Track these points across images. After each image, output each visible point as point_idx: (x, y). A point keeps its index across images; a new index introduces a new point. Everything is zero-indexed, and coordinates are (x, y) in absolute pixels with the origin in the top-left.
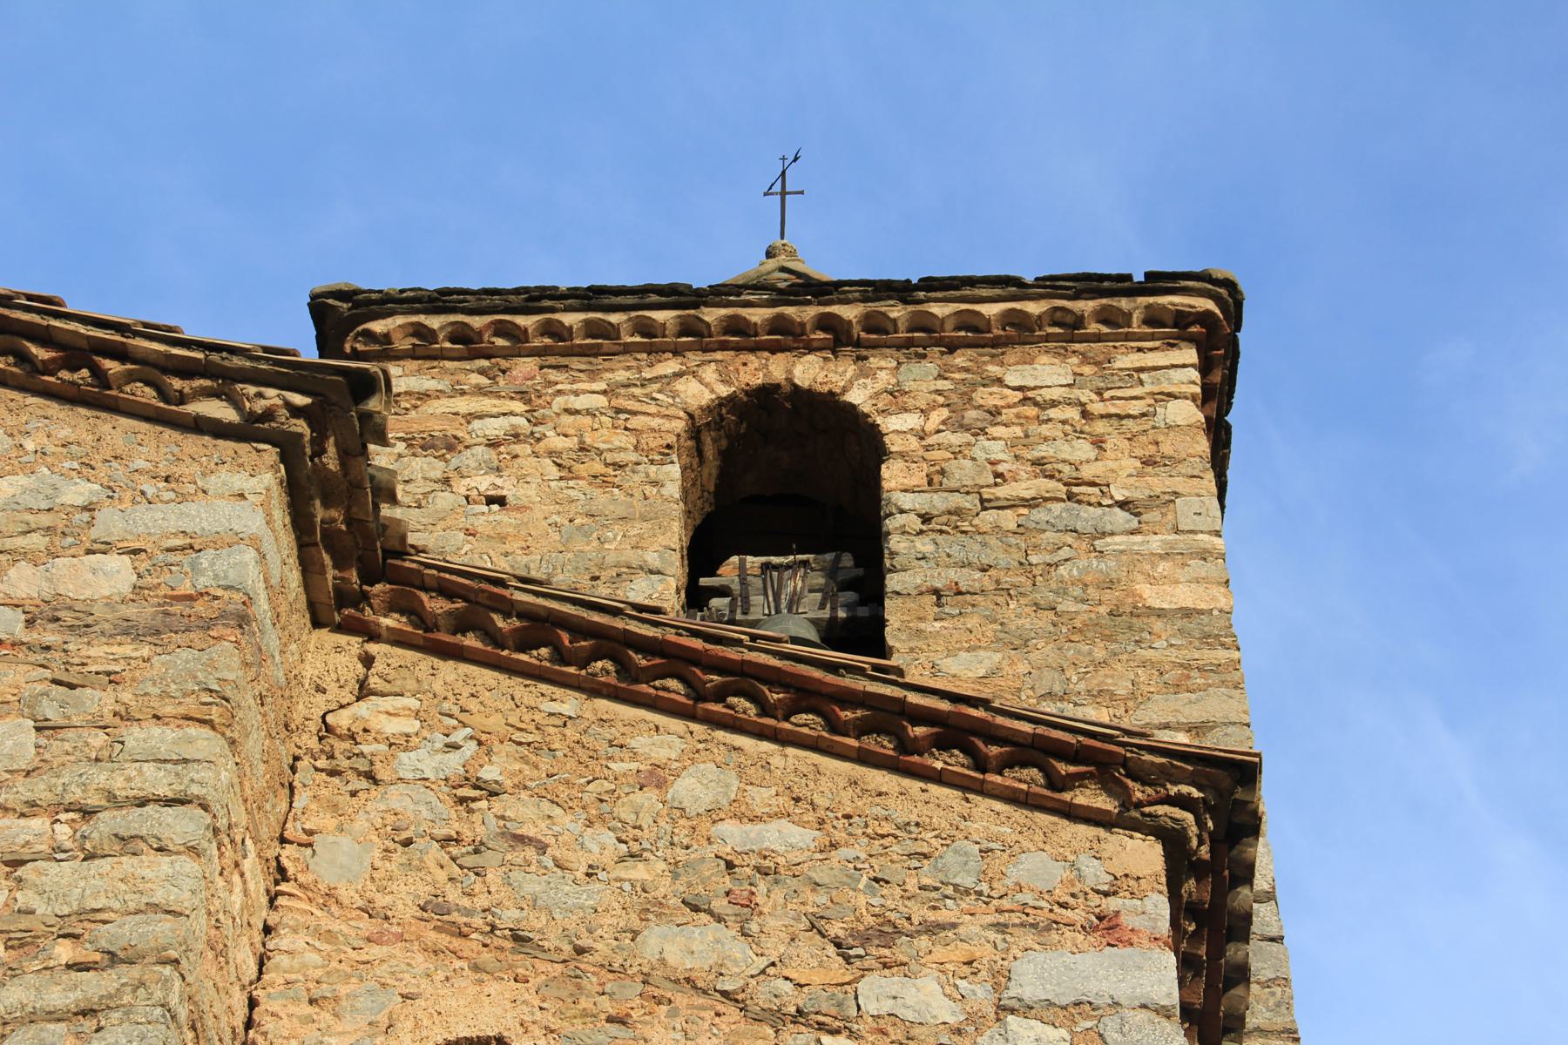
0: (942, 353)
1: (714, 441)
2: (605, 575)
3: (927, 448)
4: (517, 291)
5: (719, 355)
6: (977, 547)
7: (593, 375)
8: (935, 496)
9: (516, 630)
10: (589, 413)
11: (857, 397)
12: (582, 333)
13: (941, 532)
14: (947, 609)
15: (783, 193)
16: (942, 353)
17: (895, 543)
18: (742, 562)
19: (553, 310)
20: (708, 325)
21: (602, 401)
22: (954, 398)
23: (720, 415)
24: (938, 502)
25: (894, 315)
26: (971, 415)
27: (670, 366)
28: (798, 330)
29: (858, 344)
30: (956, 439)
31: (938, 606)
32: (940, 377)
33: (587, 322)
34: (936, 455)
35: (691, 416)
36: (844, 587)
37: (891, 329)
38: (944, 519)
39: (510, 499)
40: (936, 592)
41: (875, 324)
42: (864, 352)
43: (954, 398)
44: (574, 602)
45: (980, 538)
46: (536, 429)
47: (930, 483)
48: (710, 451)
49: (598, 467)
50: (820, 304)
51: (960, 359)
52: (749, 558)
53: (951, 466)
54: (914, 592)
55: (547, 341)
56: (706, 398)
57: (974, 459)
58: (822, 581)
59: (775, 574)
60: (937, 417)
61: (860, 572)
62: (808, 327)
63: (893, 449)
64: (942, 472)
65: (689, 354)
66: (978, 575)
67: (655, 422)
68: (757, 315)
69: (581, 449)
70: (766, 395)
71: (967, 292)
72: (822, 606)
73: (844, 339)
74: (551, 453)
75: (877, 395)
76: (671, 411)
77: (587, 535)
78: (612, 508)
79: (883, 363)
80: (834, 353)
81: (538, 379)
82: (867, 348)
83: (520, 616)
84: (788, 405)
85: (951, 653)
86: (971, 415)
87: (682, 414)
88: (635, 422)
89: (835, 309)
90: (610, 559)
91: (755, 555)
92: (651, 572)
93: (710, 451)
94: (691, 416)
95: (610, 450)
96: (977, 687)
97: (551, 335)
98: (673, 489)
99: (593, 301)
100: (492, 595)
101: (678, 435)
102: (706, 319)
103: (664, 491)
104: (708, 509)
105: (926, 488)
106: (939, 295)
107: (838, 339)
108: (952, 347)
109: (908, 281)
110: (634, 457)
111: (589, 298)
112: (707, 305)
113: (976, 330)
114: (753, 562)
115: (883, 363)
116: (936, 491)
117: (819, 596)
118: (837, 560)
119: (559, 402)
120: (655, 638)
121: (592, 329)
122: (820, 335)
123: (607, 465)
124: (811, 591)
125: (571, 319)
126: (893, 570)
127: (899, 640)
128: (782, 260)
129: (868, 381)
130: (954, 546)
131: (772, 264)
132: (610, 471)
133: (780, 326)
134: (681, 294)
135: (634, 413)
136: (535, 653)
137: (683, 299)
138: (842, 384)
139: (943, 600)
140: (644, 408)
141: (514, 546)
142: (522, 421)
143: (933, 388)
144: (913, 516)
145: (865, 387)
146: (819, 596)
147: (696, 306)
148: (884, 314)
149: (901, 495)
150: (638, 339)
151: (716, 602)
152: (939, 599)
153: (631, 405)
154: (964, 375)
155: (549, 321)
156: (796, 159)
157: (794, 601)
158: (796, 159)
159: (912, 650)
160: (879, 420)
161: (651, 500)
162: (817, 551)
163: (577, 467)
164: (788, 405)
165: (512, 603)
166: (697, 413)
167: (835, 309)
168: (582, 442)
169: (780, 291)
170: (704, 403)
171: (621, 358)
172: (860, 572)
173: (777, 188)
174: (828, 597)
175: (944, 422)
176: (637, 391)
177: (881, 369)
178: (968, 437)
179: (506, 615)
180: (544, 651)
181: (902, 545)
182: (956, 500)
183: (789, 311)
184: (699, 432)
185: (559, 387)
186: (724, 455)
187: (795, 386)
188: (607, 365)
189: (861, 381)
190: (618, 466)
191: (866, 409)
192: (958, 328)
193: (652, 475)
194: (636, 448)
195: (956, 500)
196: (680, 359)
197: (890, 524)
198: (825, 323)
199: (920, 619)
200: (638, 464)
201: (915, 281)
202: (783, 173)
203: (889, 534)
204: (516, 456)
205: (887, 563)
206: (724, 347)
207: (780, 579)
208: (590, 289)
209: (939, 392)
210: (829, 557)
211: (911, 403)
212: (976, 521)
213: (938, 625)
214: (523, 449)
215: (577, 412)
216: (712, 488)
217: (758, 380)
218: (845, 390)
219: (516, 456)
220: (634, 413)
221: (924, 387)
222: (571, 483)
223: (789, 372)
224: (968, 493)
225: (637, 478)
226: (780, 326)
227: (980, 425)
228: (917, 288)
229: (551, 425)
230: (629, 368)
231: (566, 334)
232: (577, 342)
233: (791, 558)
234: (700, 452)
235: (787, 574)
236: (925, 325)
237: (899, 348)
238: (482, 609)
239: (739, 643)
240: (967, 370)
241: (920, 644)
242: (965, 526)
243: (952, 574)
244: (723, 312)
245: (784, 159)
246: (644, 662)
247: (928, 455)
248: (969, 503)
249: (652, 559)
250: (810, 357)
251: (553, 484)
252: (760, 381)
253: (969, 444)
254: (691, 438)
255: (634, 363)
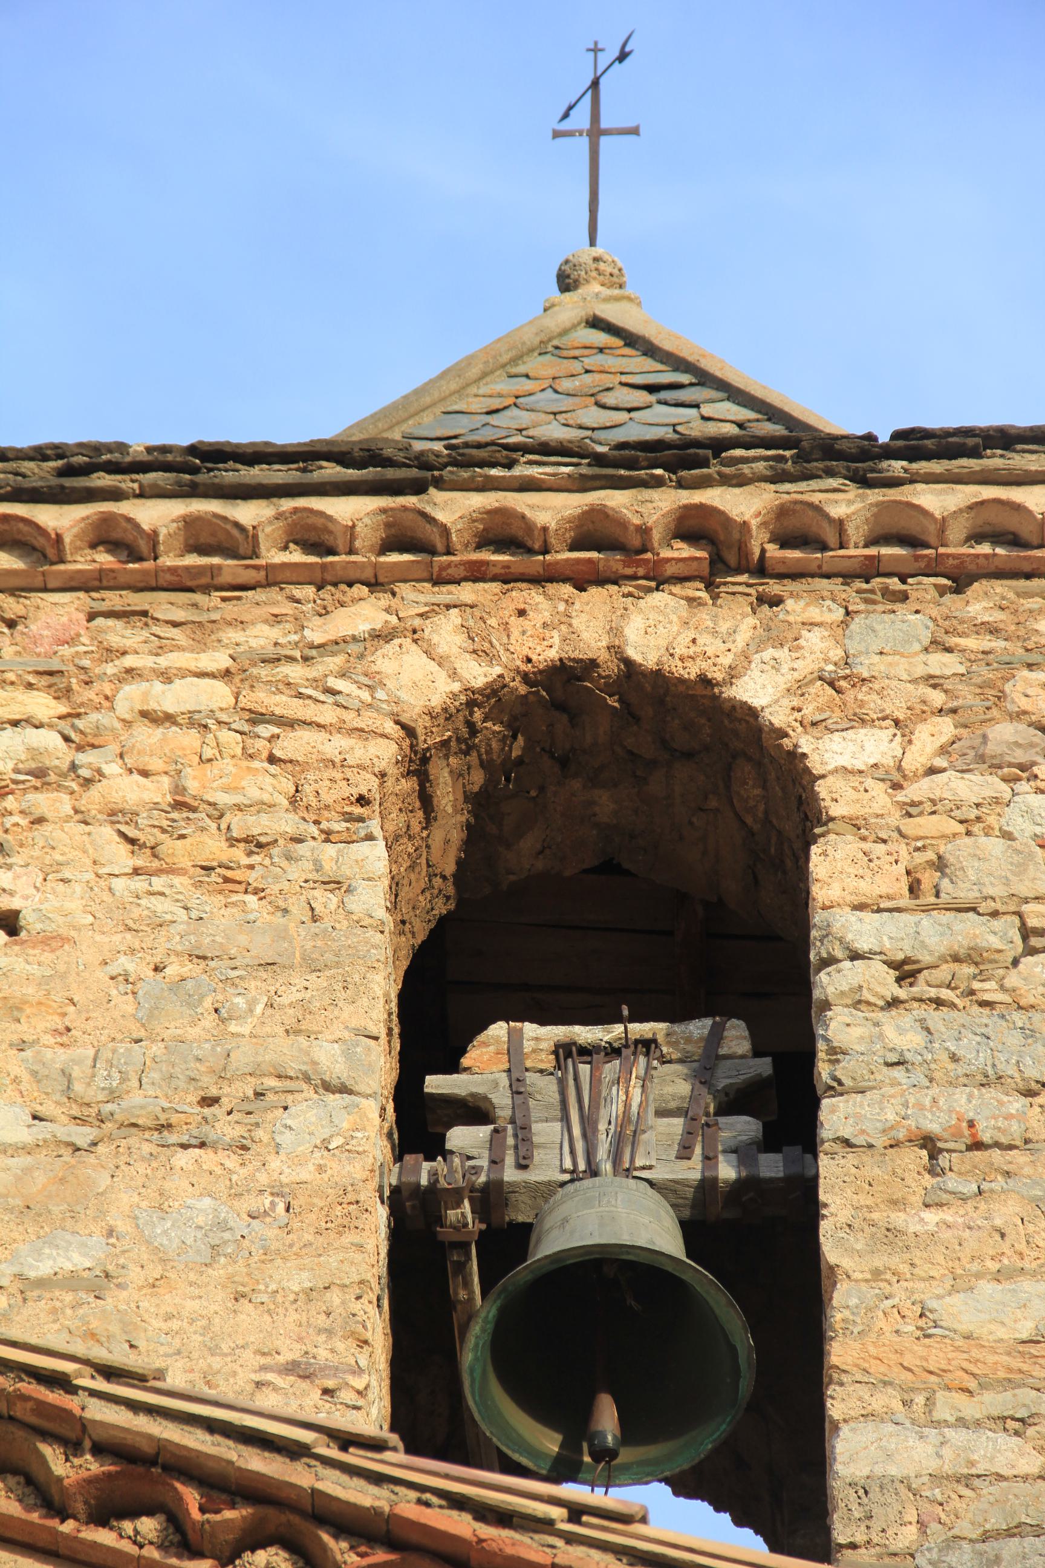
0: (942, 591)
1: (457, 775)
2: (232, 1093)
3: (910, 810)
4: (40, 454)
5: (467, 592)
6: (1014, 1039)
7: (203, 632)
8: (926, 922)
9: (90, 1481)
10: (197, 722)
11: (760, 690)
12: (179, 543)
13: (939, 1003)
14: (952, 1182)
15: (596, 133)
16: (942, 591)
17: (840, 1027)
18: (515, 1038)
19: (116, 495)
20: (445, 531)
21: (219, 694)
22: (967, 696)
23: (470, 725)
24: (930, 935)
25: (837, 511)
26: (1004, 734)
27: (364, 614)
28: (636, 542)
29: (761, 569)
30: (969, 787)
31: (932, 1172)
32: (937, 645)
33: (189, 523)
34: (925, 825)
35: (409, 731)
36: (733, 1103)
37: (832, 539)
38: (944, 972)
39: (28, 918)
40: (929, 1143)
41: (798, 532)
42: (774, 587)
43: (967, 696)
44: (212, 1426)
45: (1019, 1018)
46: (81, 758)
47: (914, 889)
48: (447, 794)
49: (214, 848)
50: (681, 485)
51: (981, 603)
52: (530, 1029)
53: (959, 851)
54: (880, 1142)
55: (104, 559)
56: (441, 690)
57: (1007, 836)
58: (684, 1088)
59: (584, 1069)
60: (933, 734)
61: (764, 1066)
62: (656, 535)
63: (835, 810)
64: (940, 865)
65: (403, 589)
66: (1017, 1104)
67: (334, 746)
68: (550, 510)
69: (178, 805)
70: (563, 687)
71: (995, 461)
72: (685, 1152)
73: (732, 559)
74: (113, 814)
75: (799, 688)
76: (366, 721)
77: (192, 1002)
78: (243, 939)
79: (814, 613)
80: (710, 586)
81: (87, 642)
82: (781, 576)
83: (99, 1450)
84: (613, 702)
85: (960, 1283)
86: (1004, 734)
87: (390, 727)
88: (292, 744)
89: (714, 497)
90: (242, 1058)
91: (543, 1023)
92: (327, 1087)
93: (447, 794)
94: (409, 731)
95: (239, 808)
96: (1017, 1363)
97: (113, 545)
98: (372, 900)
99: (202, 478)
100: (42, 1407)
101: (383, 775)
102: (441, 516)
103: (355, 904)
104: (441, 908)
105: (905, 901)
106: (936, 467)
107: (720, 557)
108: (960, 580)
109: (870, 437)
110: (287, 823)
111: (195, 470)
112: (440, 484)
113: (1015, 541)
114: (541, 1038)
115: (814, 613)
116: (926, 909)
117: (677, 1124)
118: (716, 1036)
119: (130, 697)
120: (377, 1512)
121: (201, 537)
122: (683, 550)
123: (233, 842)
124: (661, 1113)
125: (157, 515)
126: (837, 1088)
127: (851, 1252)
128: (592, 297)
129: (783, 654)
130: (964, 1035)
131: (572, 308)
132: (238, 853)
133: (594, 533)
134: (388, 462)
135: (290, 724)
136: (128, 1526)
137: (391, 473)
138: (727, 660)
139: (943, 1160)
140: (309, 712)
141: (37, 1026)
142: (50, 739)
143: (920, 671)
144: (877, 967)
145: (776, 663)
146: (677, 1124)
147: (419, 488)
148: (817, 509)
149: (853, 917)
150: (296, 556)
151: (462, 1137)
152: (932, 1157)
153: (283, 704)
154: (986, 642)
155: (107, 521)
156: (623, 56)
157: (627, 1136)
158: (623, 56)
159: (877, 1274)
160: (806, 744)
161: (327, 923)
162: (676, 1013)
163: (169, 846)
164: (613, 702)
165: (83, 1425)
166: (421, 725)
167: (714, 497)
168: (179, 789)
169: (599, 460)
170: (437, 701)
171: (259, 595)
172: (764, 1066)
173: (581, 118)
174: (696, 1132)
175: (943, 751)
176: (295, 672)
177: (812, 625)
178: (993, 785)
179: (72, 1447)
180: (148, 1526)
181: (857, 1032)
182: (970, 930)
183: (617, 500)
184: (425, 760)
185: (129, 661)
186: (481, 804)
187: (628, 662)
188: (230, 610)
189: (769, 653)
190: (257, 845)
191: (778, 717)
192: (977, 537)
193: (329, 867)
194: (293, 801)
195: (970, 930)
196: (385, 600)
197: (828, 983)
198: (693, 527)
199: (894, 1203)
200: (298, 840)
201: (884, 438)
202: (595, 84)
203: (826, 1005)
204: (40, 820)
205: (823, 1070)
206: (477, 574)
207: (595, 1080)
208: (193, 450)
209: (933, 681)
210: (699, 1028)
211: (873, 703)
212: (1013, 979)
213: (932, 1217)
214: (53, 803)
215: (169, 719)
216: (450, 868)
217: (549, 653)
218: (733, 674)
219: (40, 820)
220: (290, 724)
221: (901, 668)
222: (158, 883)
223: (615, 631)
224: (995, 914)
225: (296, 872)
226: (594, 533)
227: (1020, 756)
228: (889, 453)
229: (114, 748)
230: (277, 619)
231: (143, 546)
232: (168, 561)
233: (618, 1029)
234: (426, 801)
235: (611, 1069)
236: (905, 533)
237: (847, 577)
238: (20, 1433)
239: (545, 1525)
240: (994, 630)
241: (896, 1262)
242: (989, 990)
243: (964, 1102)
244: (477, 501)
245: (596, 50)
246: (352, 1558)
247: (910, 826)
248: (998, 937)
249: (329, 1058)
250: (659, 598)
251: (119, 884)
252: (553, 654)
253: (997, 801)
254: (409, 773)
255: (287, 608)
